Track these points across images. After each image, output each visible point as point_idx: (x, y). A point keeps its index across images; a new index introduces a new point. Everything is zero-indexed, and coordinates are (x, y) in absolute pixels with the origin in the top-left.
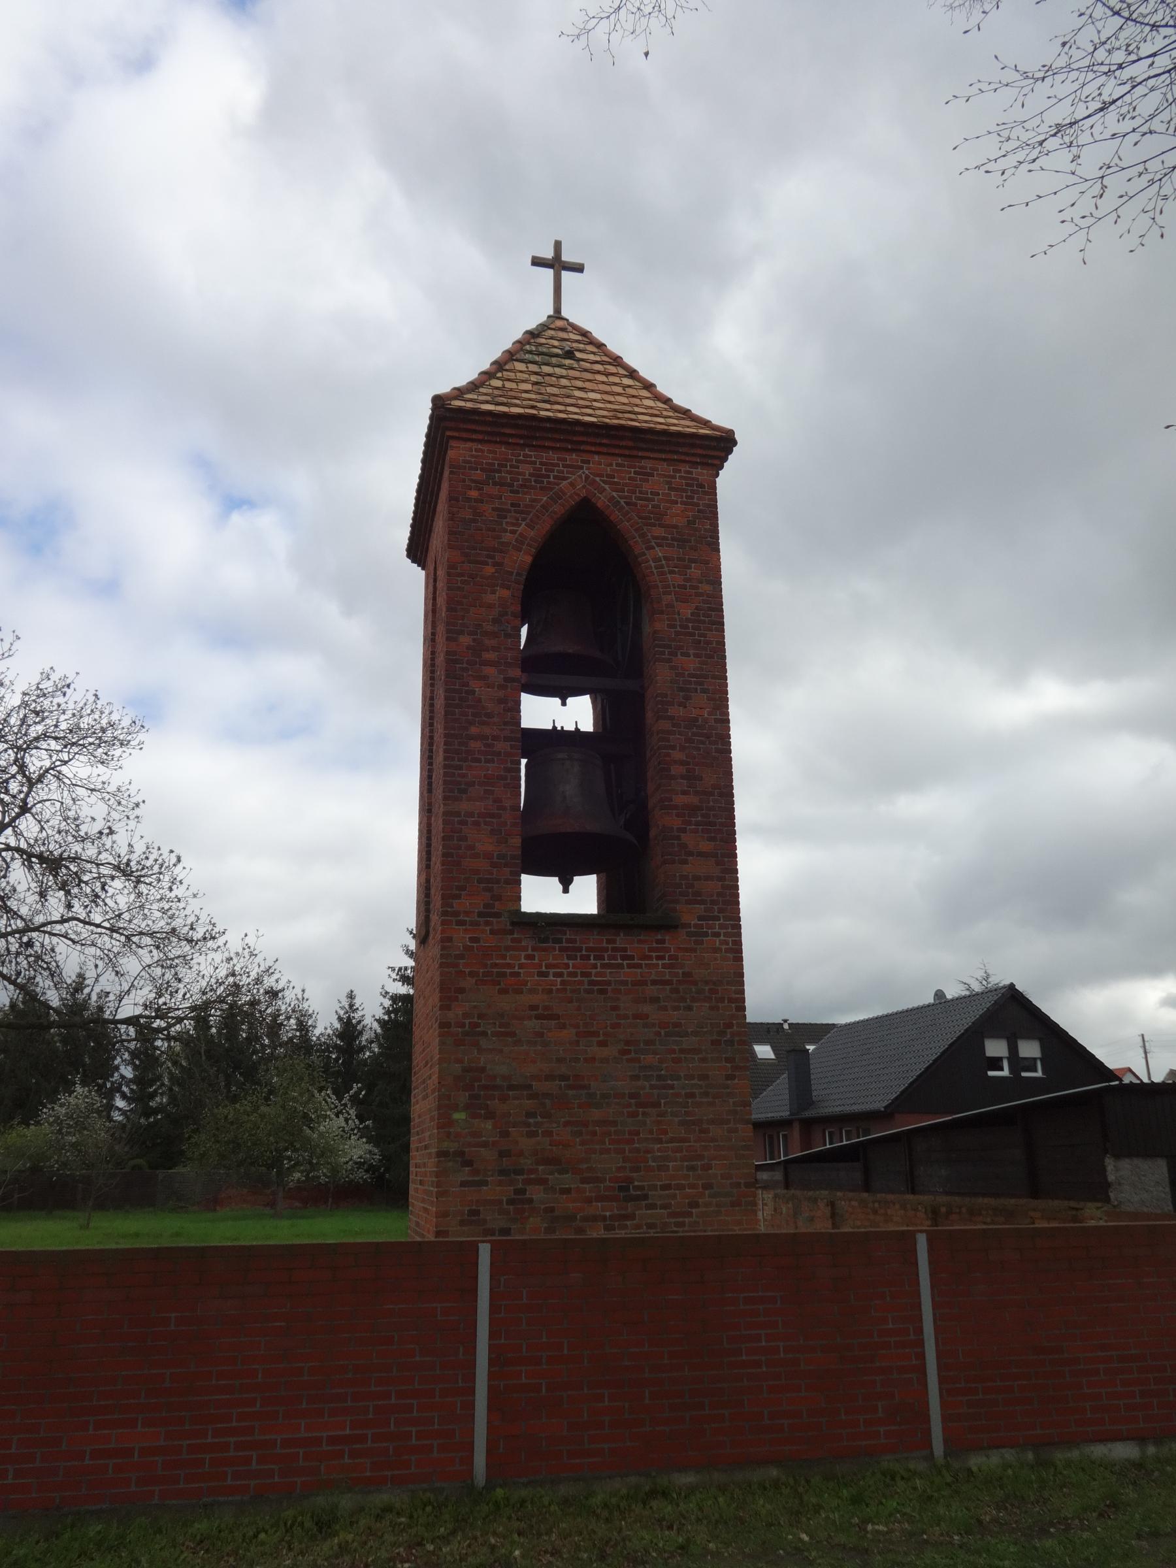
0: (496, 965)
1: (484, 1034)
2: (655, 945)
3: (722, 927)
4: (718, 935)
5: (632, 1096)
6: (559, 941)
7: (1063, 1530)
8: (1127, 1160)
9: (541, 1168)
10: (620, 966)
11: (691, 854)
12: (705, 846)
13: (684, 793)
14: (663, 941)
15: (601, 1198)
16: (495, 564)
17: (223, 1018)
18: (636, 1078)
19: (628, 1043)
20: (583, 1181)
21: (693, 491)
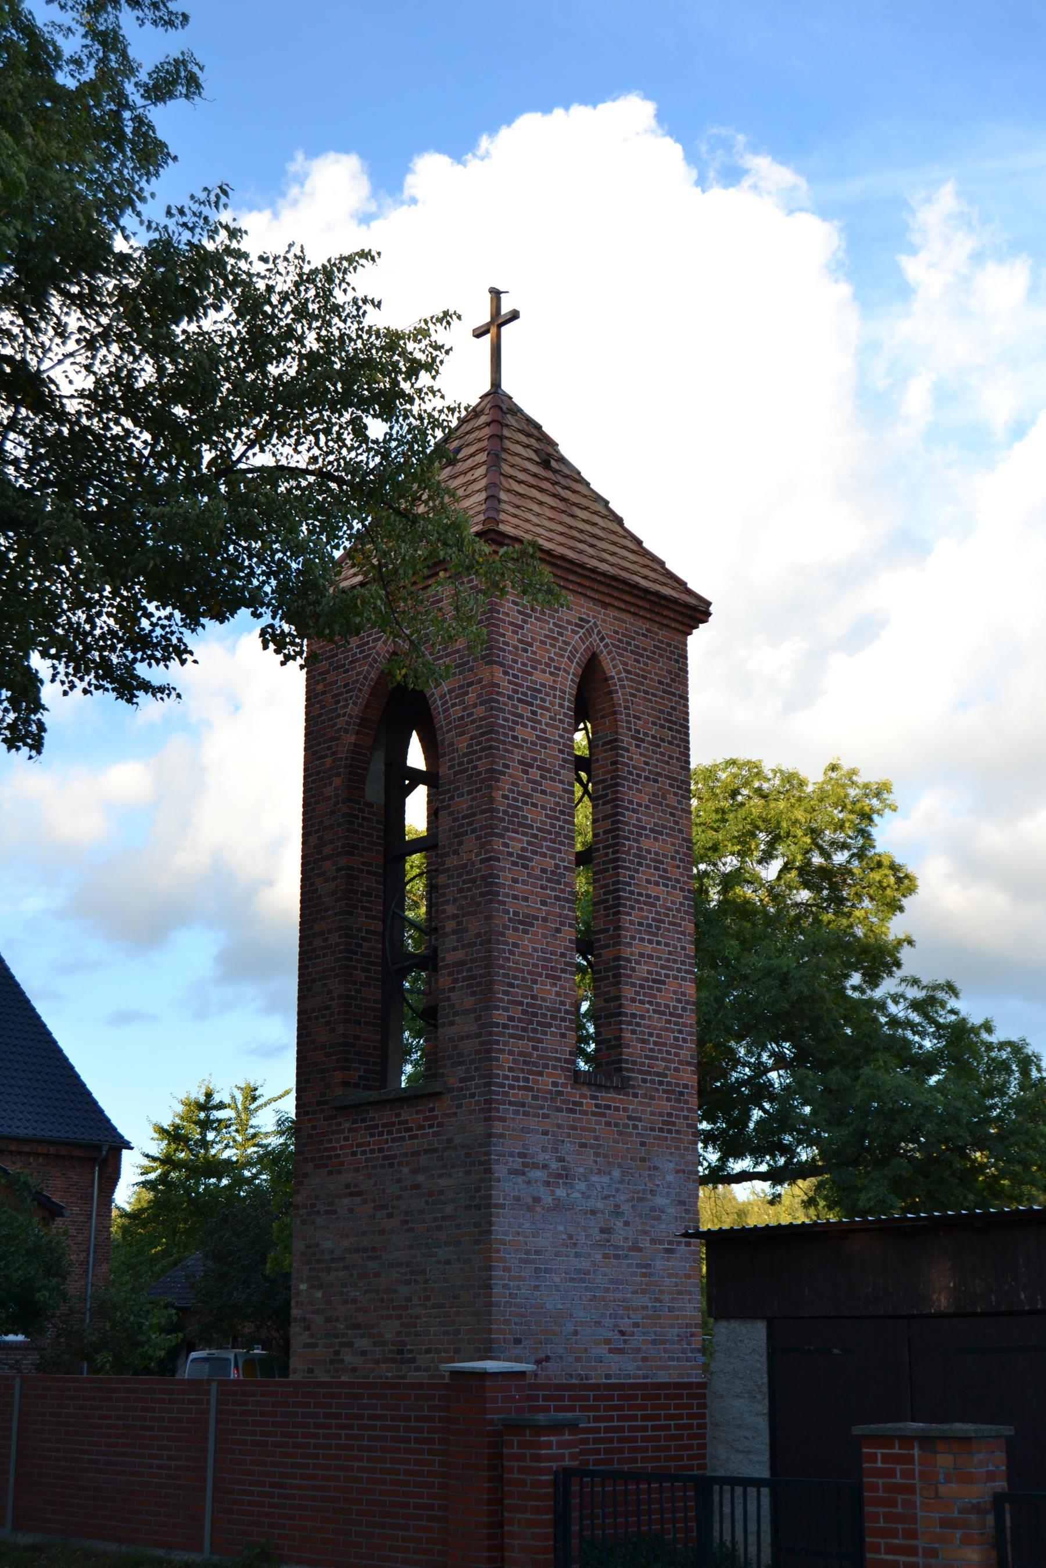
0: (326, 1149)
1: (318, 1213)
2: (428, 1114)
3: (477, 1087)
4: (472, 1095)
5: (409, 1265)
6: (364, 1120)
7: (577, 1073)
8: (783, 1223)
9: (349, 1332)
10: (403, 1139)
11: (456, 1014)
12: (468, 1002)
13: (455, 949)
14: (432, 1110)
15: (385, 1361)
16: (330, 798)
17: (280, 607)
18: (411, 1247)
19: (406, 1213)
20: (375, 1344)
21: (512, 792)
